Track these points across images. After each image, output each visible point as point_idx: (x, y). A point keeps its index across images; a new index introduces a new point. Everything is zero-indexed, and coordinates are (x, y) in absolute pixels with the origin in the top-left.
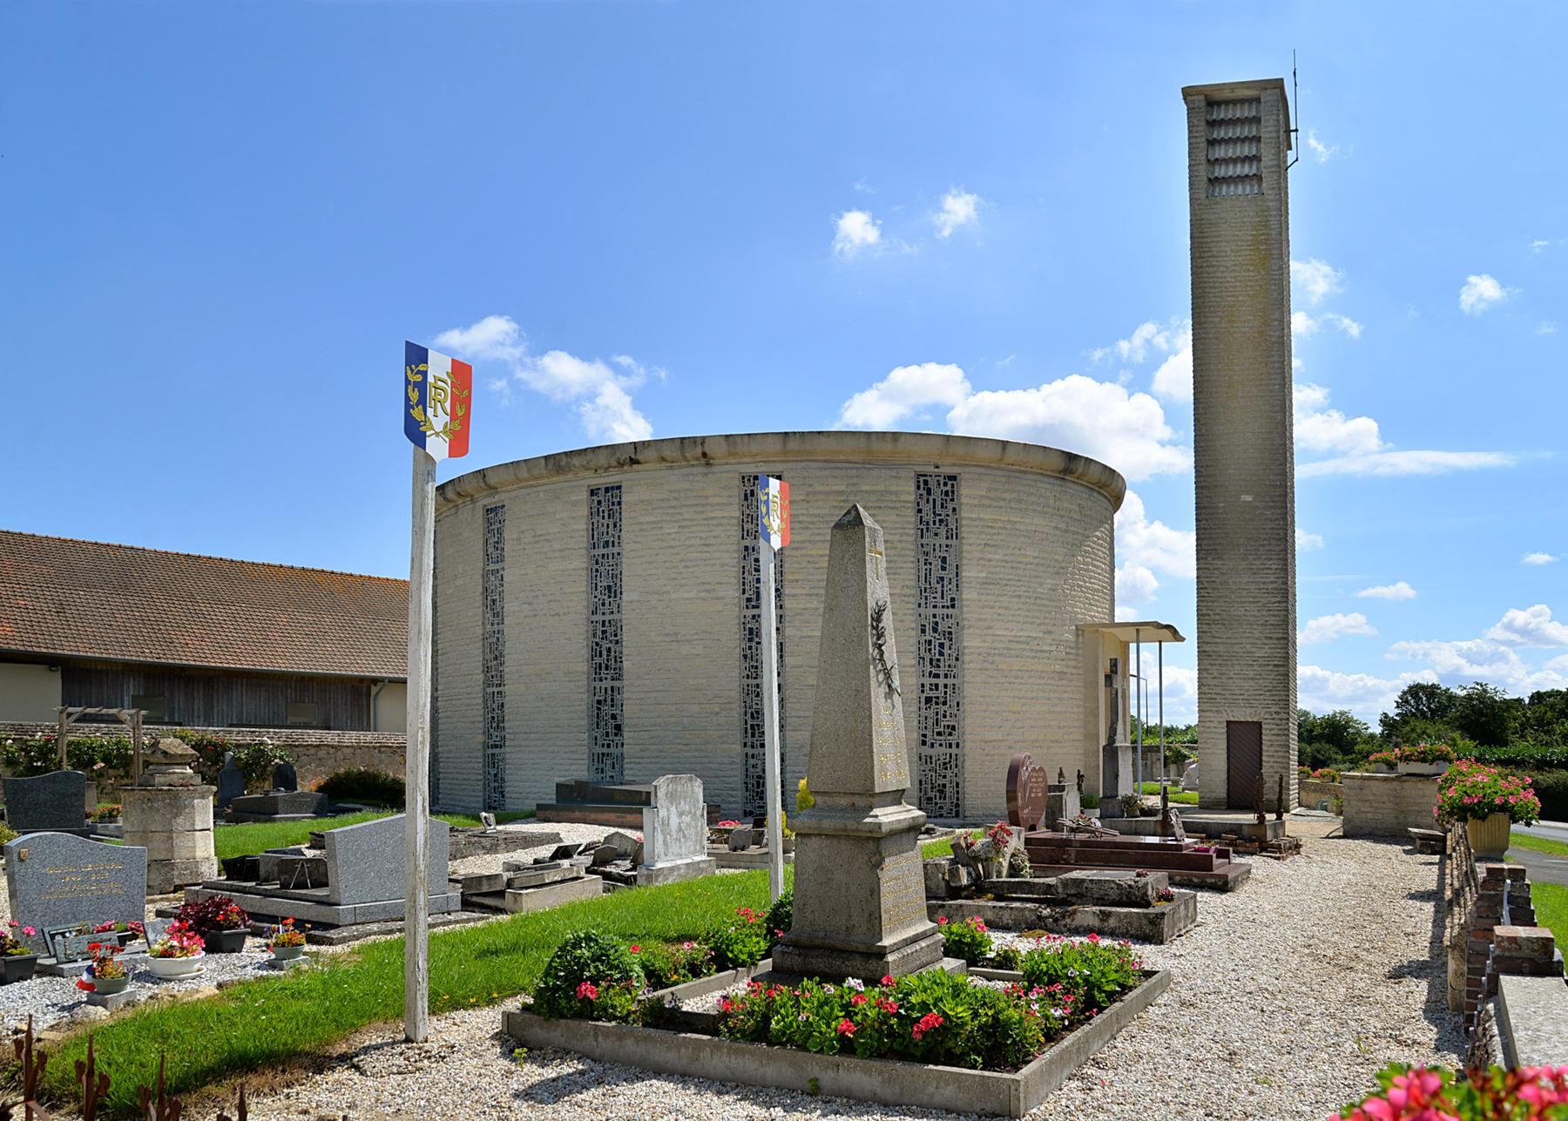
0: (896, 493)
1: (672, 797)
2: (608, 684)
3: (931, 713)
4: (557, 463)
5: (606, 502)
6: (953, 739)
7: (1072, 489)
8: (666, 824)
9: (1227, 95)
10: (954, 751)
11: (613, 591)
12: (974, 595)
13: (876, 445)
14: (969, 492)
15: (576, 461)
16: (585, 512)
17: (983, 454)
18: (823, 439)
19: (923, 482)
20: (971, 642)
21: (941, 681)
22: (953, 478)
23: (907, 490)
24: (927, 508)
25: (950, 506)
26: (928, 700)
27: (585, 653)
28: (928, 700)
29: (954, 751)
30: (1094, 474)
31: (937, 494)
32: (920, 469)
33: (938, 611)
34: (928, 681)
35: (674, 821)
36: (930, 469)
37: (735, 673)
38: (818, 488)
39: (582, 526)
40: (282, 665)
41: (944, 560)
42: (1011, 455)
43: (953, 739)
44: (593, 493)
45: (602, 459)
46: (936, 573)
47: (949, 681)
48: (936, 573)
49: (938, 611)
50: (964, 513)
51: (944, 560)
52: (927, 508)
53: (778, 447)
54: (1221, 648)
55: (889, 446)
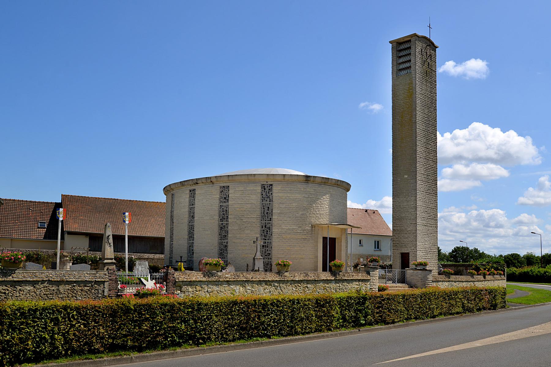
0: (256, 190)
1: (140, 264)
2: (191, 241)
3: (264, 250)
4: (182, 183)
5: (193, 192)
6: (270, 257)
7: (310, 185)
8: (138, 269)
9: (402, 41)
10: (270, 260)
11: (193, 217)
12: (276, 217)
13: (250, 178)
14: (276, 189)
15: (186, 183)
16: (188, 196)
17: (278, 178)
18: (237, 177)
19: (263, 187)
20: (275, 230)
21: (267, 241)
22: (272, 185)
23: (259, 189)
24: (264, 194)
25: (270, 193)
26: (263, 246)
27: (187, 233)
28: (263, 246)
29: (270, 260)
30: (319, 180)
31: (267, 190)
32: (262, 183)
33: (267, 222)
34: (263, 241)
35: (140, 269)
36: (265, 183)
37: (217, 239)
38: (237, 189)
39: (188, 200)
40: (149, 235)
41: (268, 208)
42: (287, 178)
43: (270, 257)
44: (190, 191)
45: (191, 183)
46: (266, 211)
47: (269, 241)
48: (266, 211)
49: (267, 222)
50: (274, 195)
51: (268, 208)
52: (264, 194)
53: (227, 179)
54: (399, 228)
55: (253, 178)
